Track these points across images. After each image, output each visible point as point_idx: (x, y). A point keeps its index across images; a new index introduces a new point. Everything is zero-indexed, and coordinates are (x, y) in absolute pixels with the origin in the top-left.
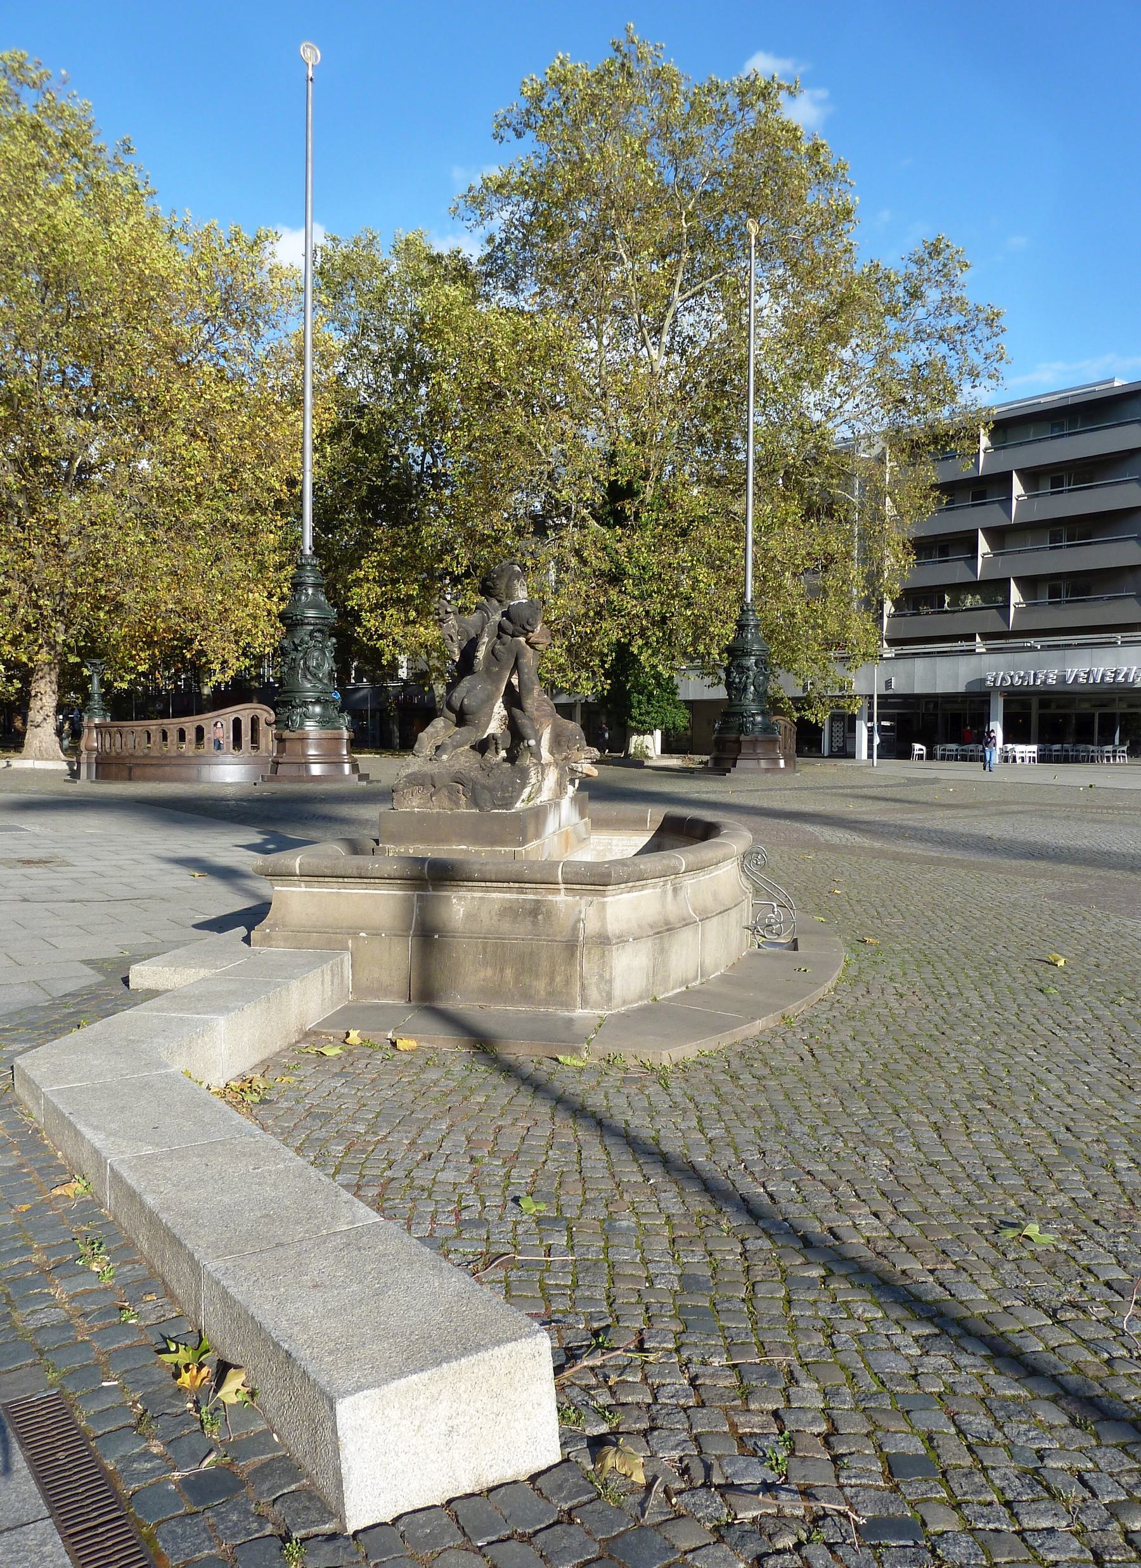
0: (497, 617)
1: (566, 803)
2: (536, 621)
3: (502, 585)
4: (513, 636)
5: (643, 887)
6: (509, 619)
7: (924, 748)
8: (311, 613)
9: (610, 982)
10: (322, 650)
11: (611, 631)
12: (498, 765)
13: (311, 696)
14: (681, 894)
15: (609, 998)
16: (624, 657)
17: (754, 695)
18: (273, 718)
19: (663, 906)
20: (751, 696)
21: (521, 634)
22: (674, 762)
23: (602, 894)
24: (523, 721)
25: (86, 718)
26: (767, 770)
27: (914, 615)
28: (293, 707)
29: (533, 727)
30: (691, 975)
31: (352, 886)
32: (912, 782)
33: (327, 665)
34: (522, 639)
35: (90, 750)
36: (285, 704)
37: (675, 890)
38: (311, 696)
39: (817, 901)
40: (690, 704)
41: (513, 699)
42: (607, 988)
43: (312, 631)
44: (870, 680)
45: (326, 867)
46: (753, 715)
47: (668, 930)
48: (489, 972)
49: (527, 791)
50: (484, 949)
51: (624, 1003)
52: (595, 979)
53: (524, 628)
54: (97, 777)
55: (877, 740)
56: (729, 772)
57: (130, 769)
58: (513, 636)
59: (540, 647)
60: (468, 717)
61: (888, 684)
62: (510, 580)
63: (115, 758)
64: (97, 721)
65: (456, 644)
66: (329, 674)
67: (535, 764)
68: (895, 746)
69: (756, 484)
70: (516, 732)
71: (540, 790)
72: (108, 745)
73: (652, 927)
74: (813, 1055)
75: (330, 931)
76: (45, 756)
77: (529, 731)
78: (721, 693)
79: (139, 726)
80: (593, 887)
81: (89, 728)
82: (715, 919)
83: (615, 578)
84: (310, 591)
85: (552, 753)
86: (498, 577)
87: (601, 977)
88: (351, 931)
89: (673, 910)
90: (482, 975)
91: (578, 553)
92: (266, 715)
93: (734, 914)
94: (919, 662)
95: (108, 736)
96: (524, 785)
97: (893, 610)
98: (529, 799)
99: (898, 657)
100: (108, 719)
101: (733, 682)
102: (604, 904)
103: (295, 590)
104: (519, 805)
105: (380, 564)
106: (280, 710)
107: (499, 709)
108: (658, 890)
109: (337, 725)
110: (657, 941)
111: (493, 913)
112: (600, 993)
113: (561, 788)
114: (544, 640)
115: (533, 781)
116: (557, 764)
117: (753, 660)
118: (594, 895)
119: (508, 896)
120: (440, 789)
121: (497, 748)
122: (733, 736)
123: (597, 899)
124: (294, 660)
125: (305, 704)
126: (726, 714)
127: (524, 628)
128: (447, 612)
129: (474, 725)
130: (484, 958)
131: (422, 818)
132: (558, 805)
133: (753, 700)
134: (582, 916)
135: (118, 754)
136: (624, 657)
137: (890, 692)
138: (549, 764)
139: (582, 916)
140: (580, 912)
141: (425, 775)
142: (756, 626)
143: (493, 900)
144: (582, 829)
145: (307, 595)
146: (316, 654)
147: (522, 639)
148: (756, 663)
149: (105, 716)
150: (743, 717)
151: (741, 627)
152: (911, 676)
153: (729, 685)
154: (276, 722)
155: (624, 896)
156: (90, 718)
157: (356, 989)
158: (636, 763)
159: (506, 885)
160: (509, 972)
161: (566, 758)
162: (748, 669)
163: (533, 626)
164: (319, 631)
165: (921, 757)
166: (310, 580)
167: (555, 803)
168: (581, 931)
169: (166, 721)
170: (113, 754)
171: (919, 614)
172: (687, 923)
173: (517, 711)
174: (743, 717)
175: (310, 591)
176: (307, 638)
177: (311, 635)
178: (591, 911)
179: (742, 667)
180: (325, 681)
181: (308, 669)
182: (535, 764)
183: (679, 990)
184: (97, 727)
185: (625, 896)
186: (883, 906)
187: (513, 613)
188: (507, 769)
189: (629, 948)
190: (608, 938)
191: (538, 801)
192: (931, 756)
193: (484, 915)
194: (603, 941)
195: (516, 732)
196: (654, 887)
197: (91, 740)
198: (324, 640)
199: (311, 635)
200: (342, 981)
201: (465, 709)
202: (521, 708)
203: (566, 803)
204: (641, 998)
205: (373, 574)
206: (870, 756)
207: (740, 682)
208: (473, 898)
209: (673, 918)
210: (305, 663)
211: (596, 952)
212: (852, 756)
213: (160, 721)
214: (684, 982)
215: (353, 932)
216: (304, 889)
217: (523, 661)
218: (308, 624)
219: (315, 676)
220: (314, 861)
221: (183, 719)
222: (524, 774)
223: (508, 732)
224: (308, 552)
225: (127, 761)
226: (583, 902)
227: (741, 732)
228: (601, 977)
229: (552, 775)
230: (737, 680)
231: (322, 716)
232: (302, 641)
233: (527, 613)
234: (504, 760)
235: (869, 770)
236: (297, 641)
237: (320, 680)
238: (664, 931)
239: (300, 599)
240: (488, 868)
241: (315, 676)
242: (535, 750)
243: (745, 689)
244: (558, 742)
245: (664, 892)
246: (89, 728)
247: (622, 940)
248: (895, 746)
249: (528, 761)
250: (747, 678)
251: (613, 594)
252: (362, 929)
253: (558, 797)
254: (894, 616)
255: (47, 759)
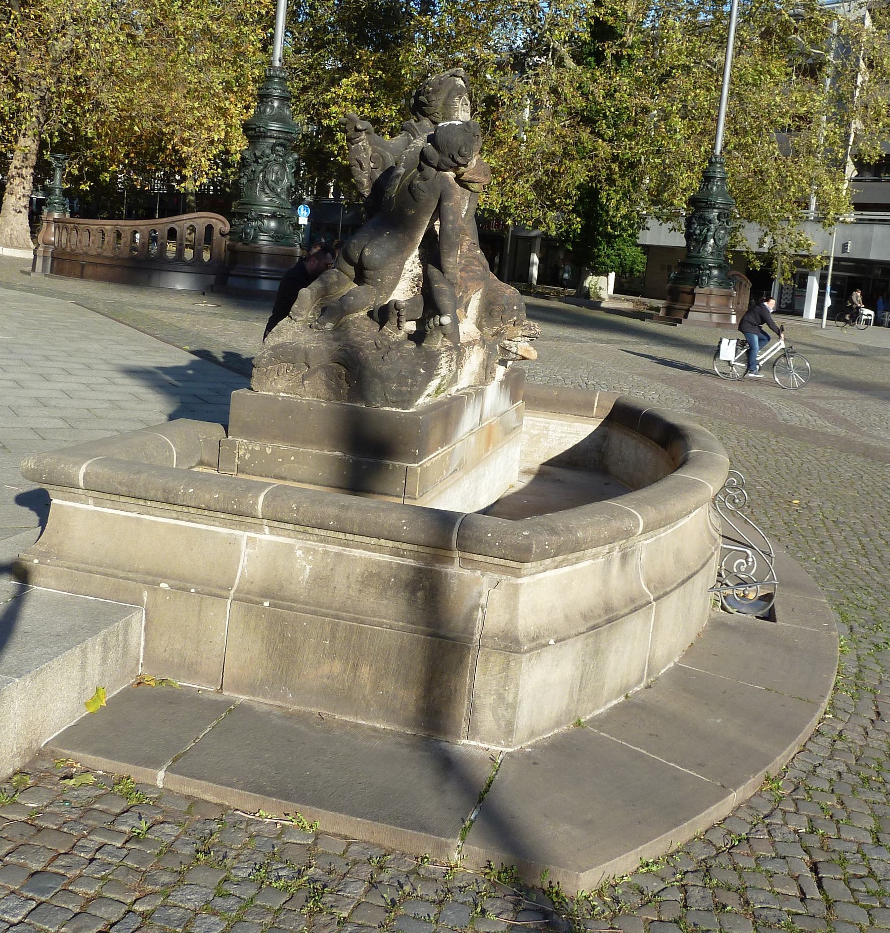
0: (420, 142)
1: (492, 390)
2: (471, 151)
3: (438, 102)
4: (438, 169)
5: (578, 560)
6: (435, 145)
7: (872, 313)
8: (274, 126)
9: (513, 707)
10: (283, 165)
11: (579, 173)
12: (399, 344)
13: (267, 210)
14: (633, 561)
15: (509, 730)
16: (589, 200)
17: (713, 248)
18: (227, 228)
19: (605, 582)
20: (709, 249)
21: (450, 168)
22: (626, 304)
23: (517, 574)
24: (440, 285)
25: (45, 211)
26: (718, 325)
27: (874, 181)
28: (249, 220)
29: (454, 295)
30: (633, 678)
31: (157, 512)
32: (863, 353)
33: (286, 181)
34: (451, 175)
35: (47, 244)
36: (241, 215)
37: (624, 557)
38: (267, 210)
39: (786, 518)
40: (647, 249)
41: (432, 254)
42: (508, 716)
43: (275, 145)
44: (826, 243)
45: (120, 483)
46: (710, 268)
47: (609, 621)
48: (337, 667)
49: (434, 384)
50: (333, 632)
51: (532, 734)
52: (490, 700)
53: (453, 160)
54: (51, 272)
55: (828, 302)
56: (680, 322)
57: (83, 266)
58: (438, 169)
59: (475, 187)
60: (368, 273)
61: (845, 246)
62: (450, 96)
63: (69, 254)
64: (56, 215)
65: (366, 174)
66: (288, 189)
67: (449, 349)
68: (842, 312)
69: (738, 37)
70: (430, 303)
71: (454, 380)
72: (64, 241)
73: (585, 617)
74: (820, 886)
75: (121, 574)
76: (15, 244)
77: (445, 301)
78: (679, 241)
79: (95, 224)
80: (502, 562)
81: (48, 222)
82: (674, 596)
83: (587, 119)
84: (276, 104)
85: (480, 327)
86: (435, 92)
87: (501, 697)
88: (150, 578)
89: (618, 586)
90: (326, 669)
91: (554, 91)
92: (220, 225)
93: (699, 580)
94: (878, 229)
95: (64, 232)
96: (429, 377)
97: (856, 173)
98: (438, 391)
99: (860, 221)
100: (68, 215)
101: (694, 233)
102: (516, 587)
103: (262, 102)
104: (422, 401)
105: (359, 86)
106: (235, 221)
107: (412, 265)
108: (601, 560)
109: (290, 241)
110: (591, 640)
111: (352, 579)
112: (497, 721)
113: (487, 370)
114: (482, 179)
115: (443, 371)
116: (483, 342)
117: (715, 213)
118: (504, 573)
119: (377, 556)
120: (315, 371)
121: (399, 322)
122: (688, 288)
123: (507, 579)
124: (253, 172)
125: (261, 217)
126: (683, 265)
127: (453, 160)
128: (357, 130)
129: (375, 285)
130: (332, 645)
131: (288, 408)
132: (480, 394)
133: (712, 253)
134: (483, 601)
135: (73, 250)
136: (589, 200)
137: (845, 255)
138: (470, 344)
139: (483, 601)
140: (480, 595)
141: (296, 349)
142: (723, 179)
143: (354, 559)
144: (512, 416)
145: (272, 107)
146: (276, 168)
147: (451, 175)
148: (718, 216)
149: (64, 212)
150: (700, 269)
151: (707, 178)
152: (867, 243)
153: (689, 236)
154: (230, 233)
155: (550, 573)
156: (50, 212)
157: (149, 660)
158: (586, 298)
159: (374, 541)
160: (365, 672)
161: (497, 334)
162: (710, 222)
163: (467, 158)
164: (281, 145)
165: (867, 322)
166: (277, 93)
167: (477, 391)
168: (479, 624)
169: (121, 222)
170: (68, 250)
171: (880, 181)
172: (637, 606)
173: (434, 271)
174: (700, 269)
175: (276, 104)
176: (268, 151)
177: (273, 148)
178: (497, 596)
179: (704, 219)
180: (283, 197)
181: (267, 182)
182: (449, 349)
183: (615, 702)
184: (55, 221)
185: (551, 573)
186: (866, 533)
187: (440, 140)
188: (408, 351)
189: (547, 655)
190: (516, 641)
191: (453, 391)
192: (878, 322)
193: (339, 580)
194: (510, 644)
195: (430, 303)
196: (595, 557)
197: (50, 234)
198: (285, 155)
199: (273, 150)
200: (125, 653)
201: (365, 261)
202: (440, 267)
203: (492, 390)
204: (558, 724)
205: (353, 93)
206: (819, 315)
207: (700, 234)
208: (326, 553)
209: (617, 600)
210: (264, 177)
211: (497, 660)
212: (800, 314)
213: (114, 222)
214: (624, 690)
215: (151, 579)
216: (92, 507)
217: (448, 204)
218: (271, 137)
219: (273, 190)
220: (104, 471)
221: (138, 222)
222: (431, 362)
223: (420, 299)
224: (277, 64)
225: (80, 258)
226: (485, 580)
227: (697, 284)
228: (501, 697)
229: (475, 359)
230: (698, 232)
231: (276, 231)
232: (263, 155)
233: (459, 139)
234: (411, 337)
235: (816, 333)
236: (258, 153)
237: (278, 195)
238: (603, 620)
239: (265, 111)
240: (349, 514)
241: (273, 190)
242: (449, 330)
243: (705, 241)
244: (489, 312)
245: (609, 562)
246: (48, 222)
247: (538, 643)
248: (842, 312)
249: (438, 343)
250: (708, 230)
251: (585, 134)
252: (165, 577)
253: (482, 383)
254: (854, 180)
255: (16, 247)
